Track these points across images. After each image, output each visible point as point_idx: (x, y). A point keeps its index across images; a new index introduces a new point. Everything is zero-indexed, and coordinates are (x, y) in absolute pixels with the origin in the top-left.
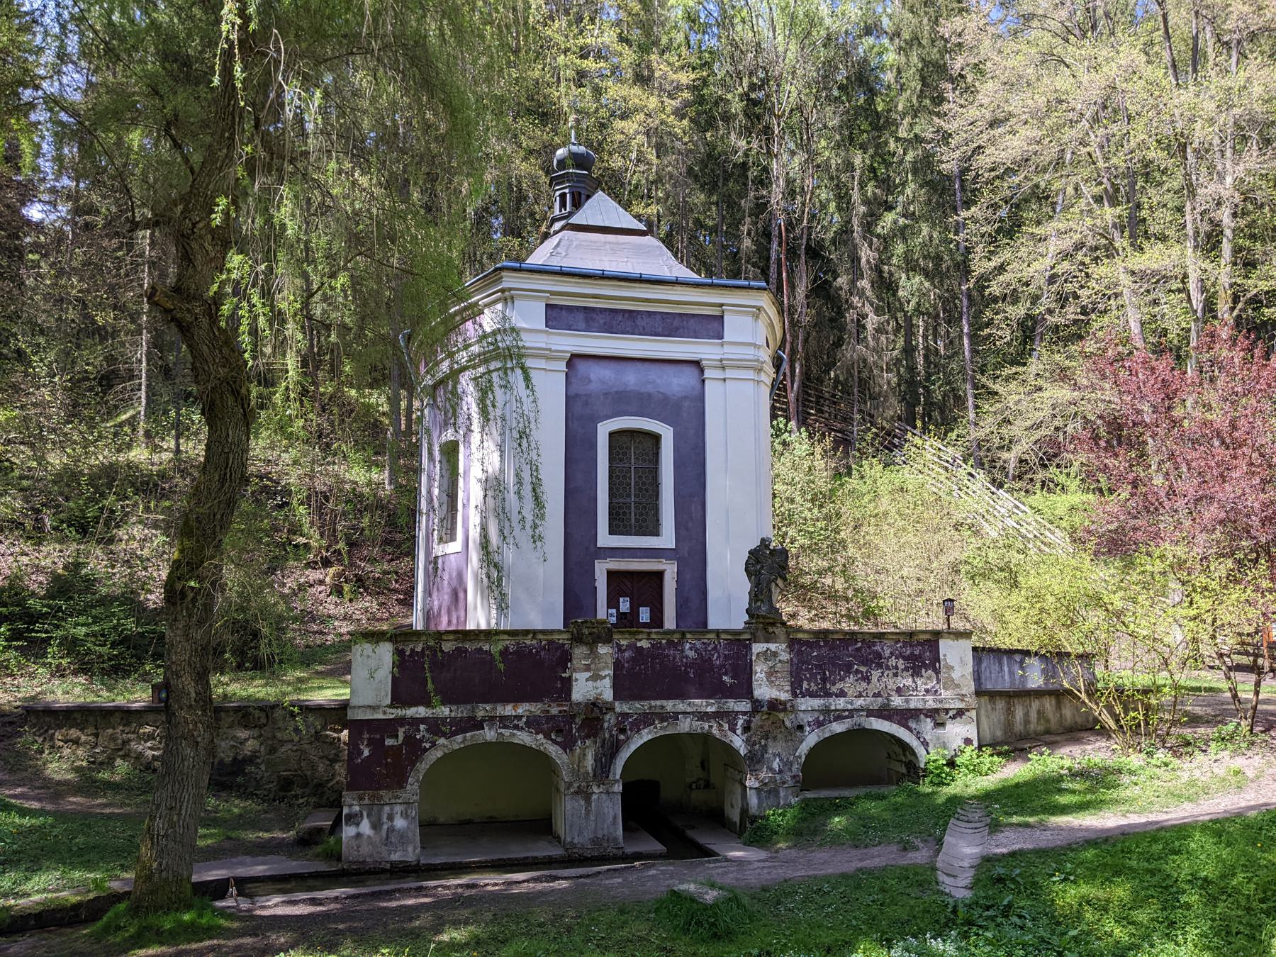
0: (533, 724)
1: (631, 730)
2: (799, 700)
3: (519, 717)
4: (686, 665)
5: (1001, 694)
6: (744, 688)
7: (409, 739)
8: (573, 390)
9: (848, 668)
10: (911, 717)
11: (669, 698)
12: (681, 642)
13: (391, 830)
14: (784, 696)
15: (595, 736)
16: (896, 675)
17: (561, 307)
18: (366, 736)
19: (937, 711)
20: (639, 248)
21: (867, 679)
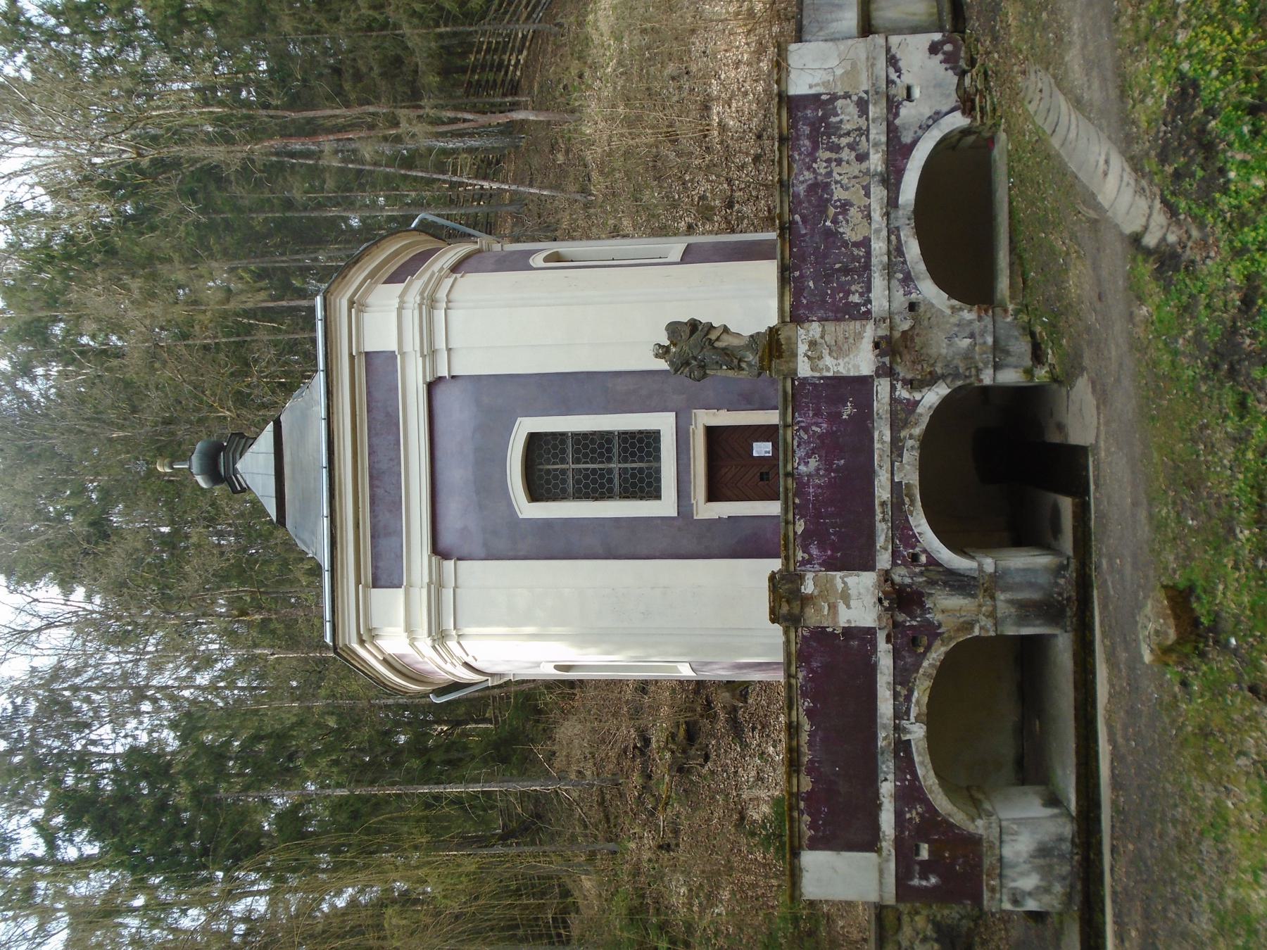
1: (913, 548)
4: (828, 470)
6: (860, 387)
10: (899, 138)
11: (872, 495)
14: (870, 332)
15: (921, 595)
17: (375, 567)
21: (845, 206)
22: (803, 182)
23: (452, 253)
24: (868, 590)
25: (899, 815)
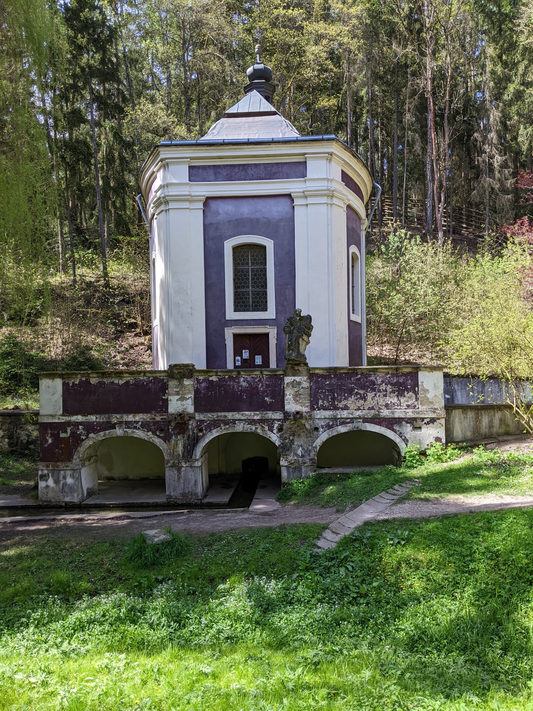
0: (145, 426)
1: (206, 430)
2: (315, 412)
3: (137, 422)
4: (241, 391)
5: (472, 408)
6: (279, 405)
7: (73, 434)
8: (208, 221)
9: (351, 392)
12: (238, 377)
13: (65, 484)
14: (304, 409)
16: (385, 396)
17: (199, 167)
18: (49, 432)
19: (415, 419)
20: (269, 122)
21: (364, 398)
22: (376, 379)
23: (359, 205)
24: (186, 409)
25: (81, 423)
